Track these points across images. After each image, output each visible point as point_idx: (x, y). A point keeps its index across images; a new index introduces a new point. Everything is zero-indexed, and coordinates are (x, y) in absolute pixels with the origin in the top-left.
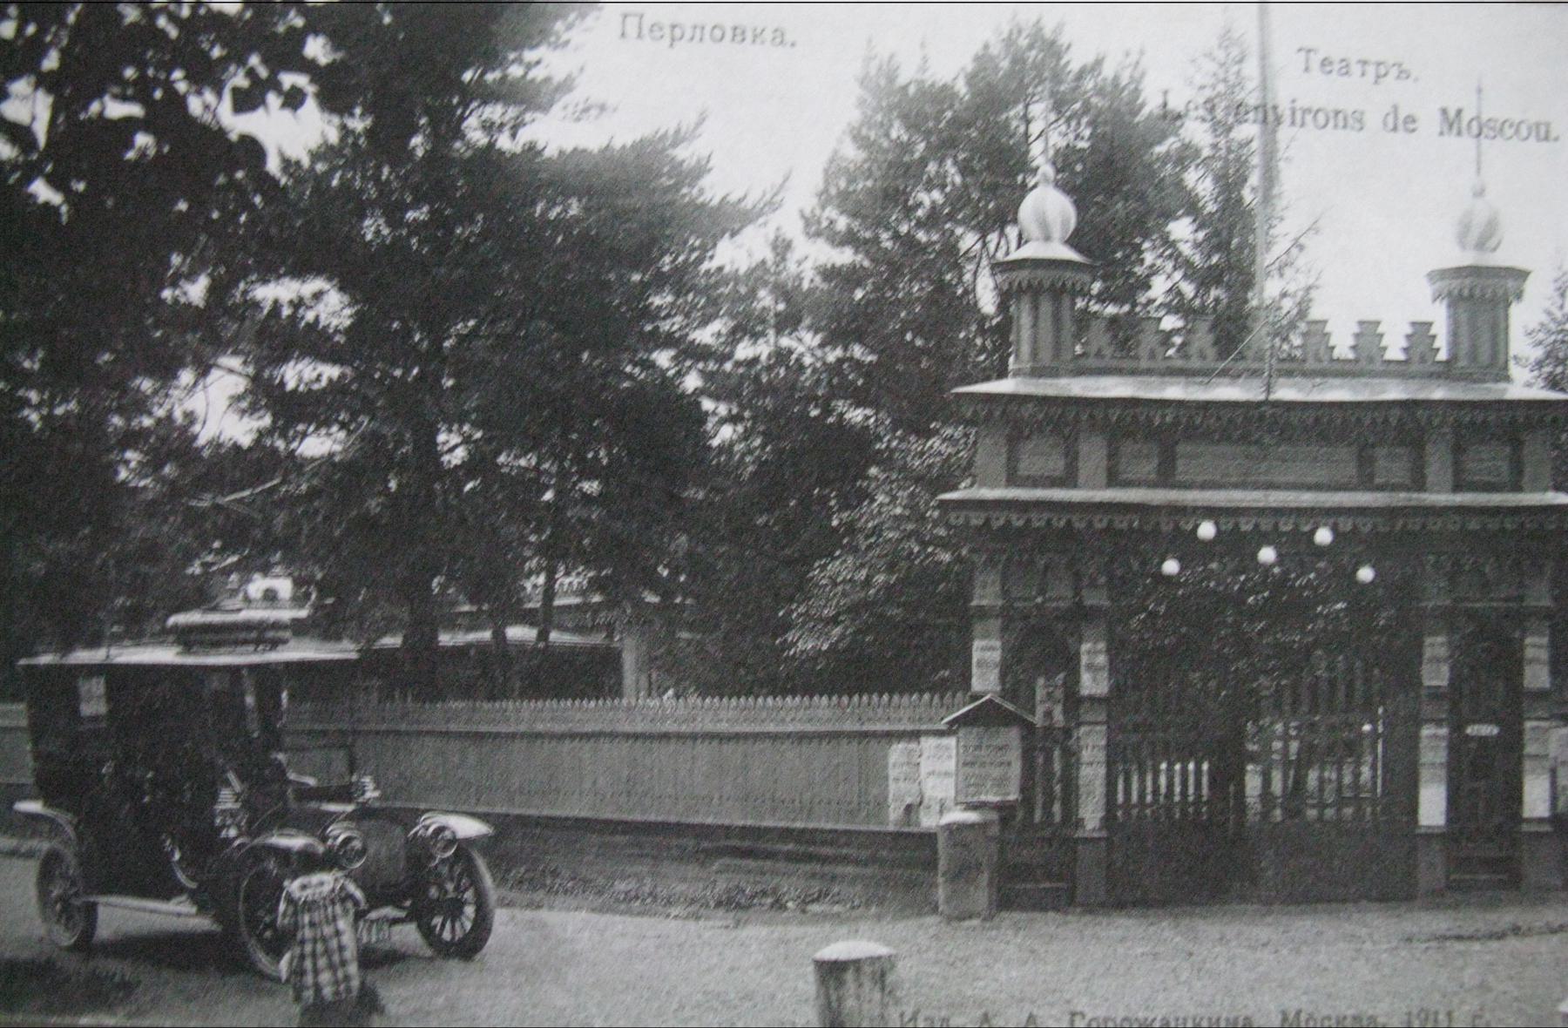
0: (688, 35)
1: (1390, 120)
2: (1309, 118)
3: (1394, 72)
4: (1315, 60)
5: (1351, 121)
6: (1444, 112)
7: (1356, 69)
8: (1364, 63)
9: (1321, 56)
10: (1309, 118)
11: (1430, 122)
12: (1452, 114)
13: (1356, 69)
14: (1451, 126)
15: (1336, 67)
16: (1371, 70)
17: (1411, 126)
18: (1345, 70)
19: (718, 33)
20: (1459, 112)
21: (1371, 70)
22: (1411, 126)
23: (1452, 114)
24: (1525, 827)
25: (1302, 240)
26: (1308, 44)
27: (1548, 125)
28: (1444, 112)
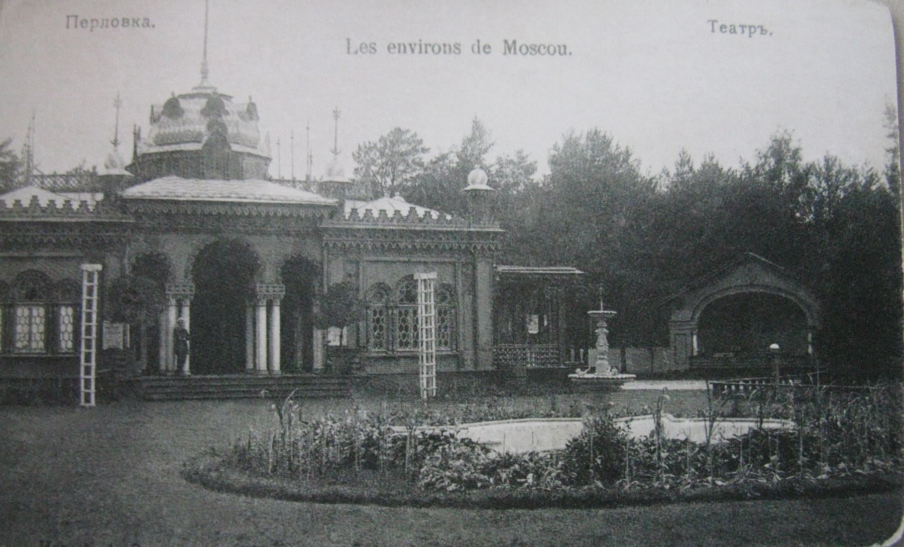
0: (100, 24)
1: (476, 49)
2: (429, 49)
3: (759, 30)
4: (717, 27)
5: (453, 48)
6: (506, 42)
7: (739, 30)
8: (743, 27)
9: (720, 23)
10: (429, 49)
11: (498, 47)
12: (510, 43)
13: (739, 30)
14: (510, 50)
15: (728, 29)
16: (747, 30)
17: (487, 50)
18: (733, 31)
19: (115, 23)
20: (514, 42)
21: (747, 30)
22: (487, 50)
23: (510, 43)
24: (344, 342)
25: (183, 104)
26: (713, 18)
27: (565, 47)
28: (506, 42)
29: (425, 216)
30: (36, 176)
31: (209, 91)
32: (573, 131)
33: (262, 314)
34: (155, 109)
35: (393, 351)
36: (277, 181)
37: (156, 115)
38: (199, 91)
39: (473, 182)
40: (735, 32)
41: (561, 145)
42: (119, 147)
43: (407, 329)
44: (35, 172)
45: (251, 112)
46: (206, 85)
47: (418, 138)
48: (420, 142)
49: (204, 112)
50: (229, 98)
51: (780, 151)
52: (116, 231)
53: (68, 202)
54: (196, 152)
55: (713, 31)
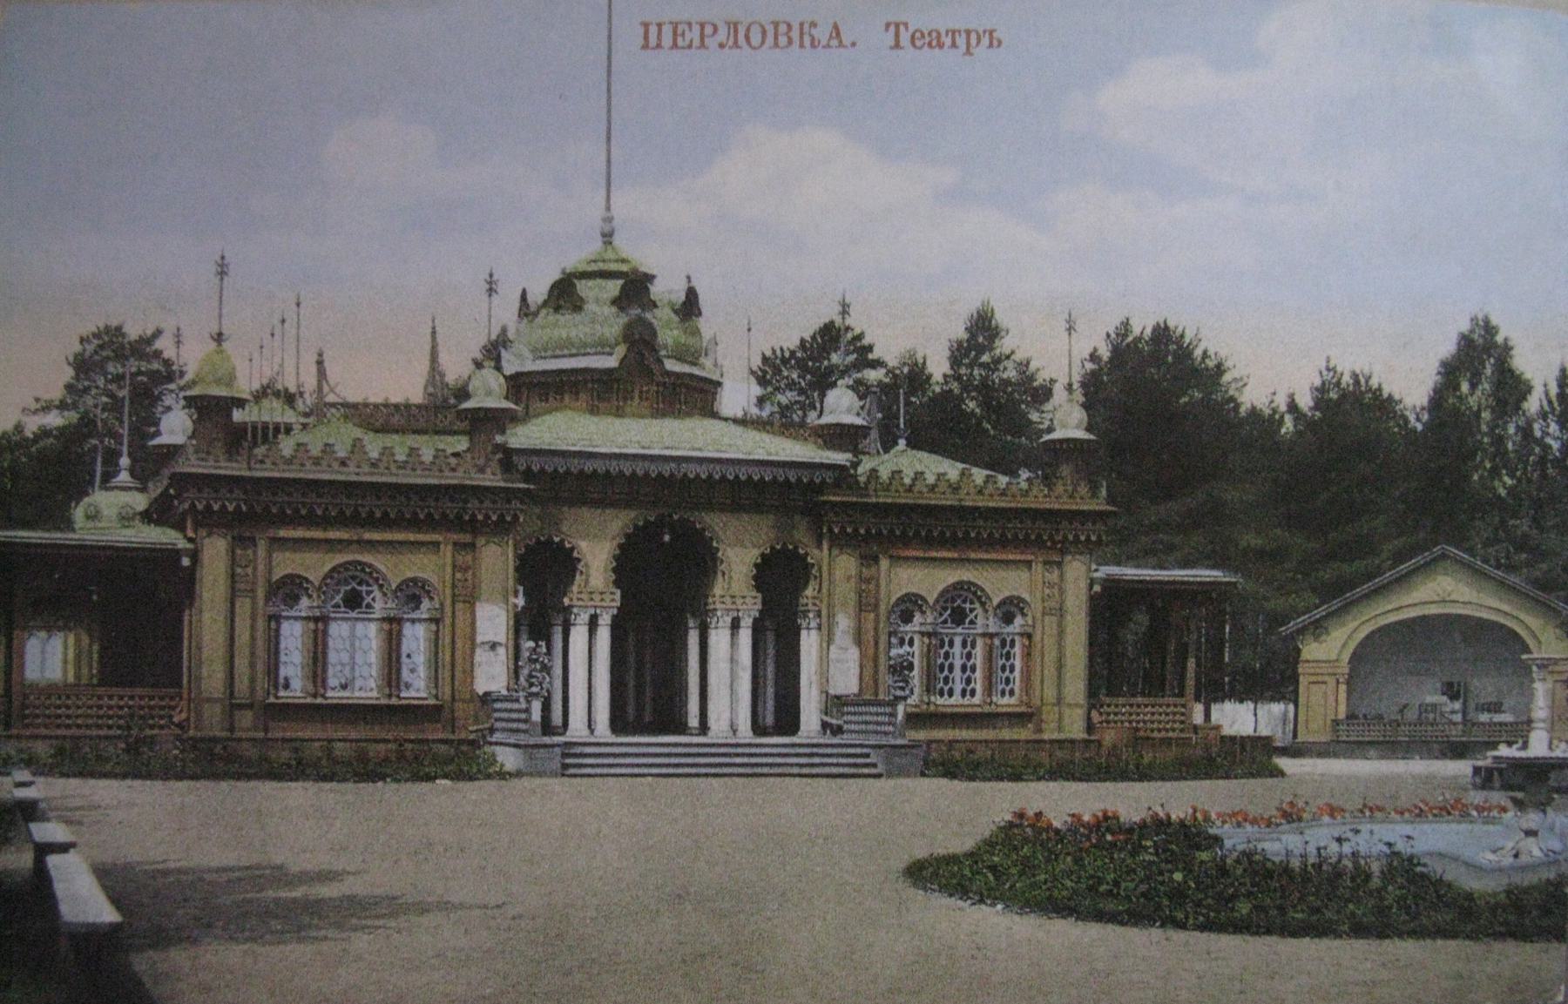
3: (985, 41)
7: (948, 41)
29: (986, 482)
30: (333, 405)
31: (624, 268)
32: (1126, 324)
33: (579, 636)
34: (530, 299)
35: (323, 696)
36: (735, 421)
37: (533, 308)
38: (601, 266)
39: (1064, 426)
40: (941, 46)
41: (1105, 353)
42: (225, 345)
43: (964, 669)
44: (331, 398)
45: (690, 307)
46: (610, 255)
47: (866, 342)
48: (870, 348)
49: (620, 302)
50: (1126, 324)
51: (563, 272)
52: (290, 494)
53: (413, 452)
54: (609, 371)
55: (897, 45)
